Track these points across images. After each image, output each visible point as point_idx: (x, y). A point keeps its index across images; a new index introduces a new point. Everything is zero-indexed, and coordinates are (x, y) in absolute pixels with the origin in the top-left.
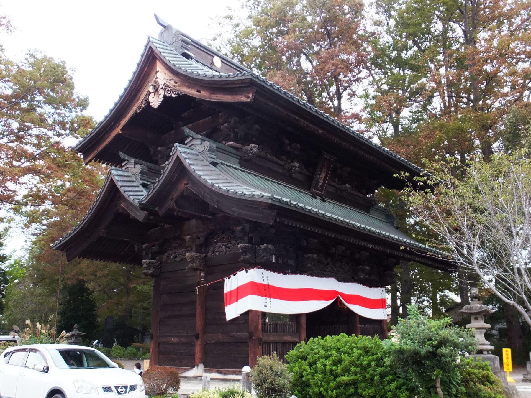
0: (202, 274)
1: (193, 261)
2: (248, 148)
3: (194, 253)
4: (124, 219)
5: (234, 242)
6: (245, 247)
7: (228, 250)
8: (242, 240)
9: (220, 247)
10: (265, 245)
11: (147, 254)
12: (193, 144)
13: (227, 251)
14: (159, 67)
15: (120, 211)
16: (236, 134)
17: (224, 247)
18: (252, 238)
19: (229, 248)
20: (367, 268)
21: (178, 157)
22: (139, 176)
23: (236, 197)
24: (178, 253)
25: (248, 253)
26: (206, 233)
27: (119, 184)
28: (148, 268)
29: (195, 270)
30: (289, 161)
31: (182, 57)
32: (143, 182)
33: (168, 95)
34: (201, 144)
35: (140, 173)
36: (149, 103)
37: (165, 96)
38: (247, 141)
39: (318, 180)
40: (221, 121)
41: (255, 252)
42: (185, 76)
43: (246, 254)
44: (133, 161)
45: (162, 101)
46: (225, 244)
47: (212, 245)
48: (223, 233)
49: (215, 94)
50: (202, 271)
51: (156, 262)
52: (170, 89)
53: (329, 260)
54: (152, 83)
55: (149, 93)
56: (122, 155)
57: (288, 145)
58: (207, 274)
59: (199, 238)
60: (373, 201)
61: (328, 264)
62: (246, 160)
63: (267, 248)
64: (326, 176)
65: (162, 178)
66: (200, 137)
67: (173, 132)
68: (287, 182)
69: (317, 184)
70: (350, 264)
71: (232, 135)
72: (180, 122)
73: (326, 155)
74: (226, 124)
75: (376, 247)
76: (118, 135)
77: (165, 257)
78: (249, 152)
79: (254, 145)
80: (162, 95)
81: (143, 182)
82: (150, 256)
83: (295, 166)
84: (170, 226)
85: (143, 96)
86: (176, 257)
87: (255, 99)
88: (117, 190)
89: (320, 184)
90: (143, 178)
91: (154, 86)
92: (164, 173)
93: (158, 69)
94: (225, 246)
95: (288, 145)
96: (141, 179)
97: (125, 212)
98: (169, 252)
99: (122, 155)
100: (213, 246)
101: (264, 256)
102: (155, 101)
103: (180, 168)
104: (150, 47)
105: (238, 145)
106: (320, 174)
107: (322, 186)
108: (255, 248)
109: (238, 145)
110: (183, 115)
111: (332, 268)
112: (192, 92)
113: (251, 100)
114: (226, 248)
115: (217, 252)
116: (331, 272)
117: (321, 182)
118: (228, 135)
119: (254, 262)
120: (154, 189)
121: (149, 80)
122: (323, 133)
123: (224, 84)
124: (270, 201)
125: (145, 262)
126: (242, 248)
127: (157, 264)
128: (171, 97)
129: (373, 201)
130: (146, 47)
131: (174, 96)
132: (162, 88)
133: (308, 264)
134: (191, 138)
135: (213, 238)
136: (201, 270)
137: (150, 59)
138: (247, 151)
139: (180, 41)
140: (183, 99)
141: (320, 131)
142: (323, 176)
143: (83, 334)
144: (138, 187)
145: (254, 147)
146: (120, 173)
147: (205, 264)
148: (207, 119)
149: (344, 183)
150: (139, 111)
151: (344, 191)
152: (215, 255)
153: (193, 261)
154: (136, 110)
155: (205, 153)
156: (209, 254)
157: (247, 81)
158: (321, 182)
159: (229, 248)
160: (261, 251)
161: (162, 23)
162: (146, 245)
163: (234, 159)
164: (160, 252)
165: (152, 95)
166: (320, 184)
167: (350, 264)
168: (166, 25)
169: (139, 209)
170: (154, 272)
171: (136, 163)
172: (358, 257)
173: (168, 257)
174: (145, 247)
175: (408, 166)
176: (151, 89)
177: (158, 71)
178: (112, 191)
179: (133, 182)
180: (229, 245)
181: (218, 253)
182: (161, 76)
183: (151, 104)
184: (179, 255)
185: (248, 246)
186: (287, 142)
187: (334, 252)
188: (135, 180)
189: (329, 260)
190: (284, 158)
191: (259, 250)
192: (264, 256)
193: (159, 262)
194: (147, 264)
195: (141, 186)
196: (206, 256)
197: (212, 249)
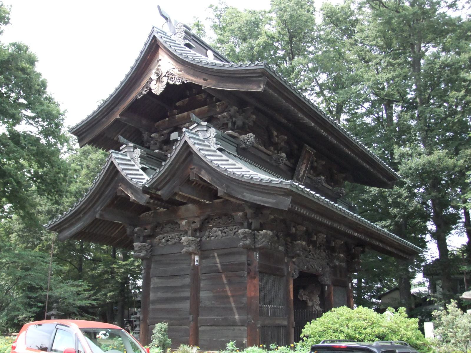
0: (197, 258)
1: (189, 245)
2: (245, 137)
3: (191, 238)
4: (121, 203)
5: (231, 227)
6: (246, 233)
7: (224, 234)
8: (241, 225)
9: (216, 232)
10: (264, 231)
11: (139, 237)
12: (198, 130)
13: (223, 236)
14: (163, 56)
15: (118, 194)
16: (234, 123)
17: (220, 232)
18: (251, 224)
19: (225, 233)
20: (342, 255)
21: (186, 142)
22: (138, 160)
23: (251, 182)
24: (171, 236)
25: (248, 238)
26: (202, 218)
27: (120, 168)
28: (140, 251)
29: (190, 254)
30: (276, 152)
31: (185, 47)
32: (143, 166)
33: (171, 83)
34: (207, 131)
35: (140, 157)
36: (150, 89)
37: (168, 84)
38: (243, 130)
39: (299, 171)
40: (218, 110)
41: (254, 238)
42: (192, 65)
43: (247, 240)
44: (132, 145)
45: (165, 89)
46: (221, 229)
47: (206, 230)
48: (220, 218)
49: (222, 83)
50: (197, 255)
51: (148, 246)
52: (173, 77)
53: (311, 247)
54: (154, 71)
55: (151, 80)
56: (122, 139)
57: (276, 136)
58: (201, 258)
59: (194, 222)
60: (341, 193)
61: (310, 251)
62: (244, 149)
63: (266, 234)
64: (306, 168)
65: (169, 162)
66: (206, 123)
67: (167, 119)
68: (275, 172)
69: (299, 175)
70: (327, 252)
71: (230, 125)
72: (174, 111)
73: (308, 148)
74: (225, 114)
75: (360, 236)
76: (117, 120)
77: (156, 240)
78: (246, 141)
79: (251, 134)
80: (165, 83)
81: (143, 166)
82: (141, 239)
83: (282, 157)
84: (165, 210)
85: (144, 83)
86: (168, 241)
87: (265, 90)
88: (117, 172)
89: (301, 175)
90: (142, 162)
91: (157, 74)
92: (171, 157)
93: (160, 57)
94: (222, 231)
95: (276, 136)
96: (141, 163)
97: (123, 194)
98: (161, 236)
99: (122, 139)
100: (208, 230)
101: (263, 242)
102: (157, 89)
103: (187, 152)
104: (154, 36)
105: (236, 134)
106: (302, 165)
107: (302, 177)
108: (254, 234)
109: (236, 134)
110: (177, 104)
111: (313, 255)
112: (198, 81)
113: (262, 90)
114: (222, 233)
115: (212, 236)
116: (313, 259)
117: (302, 173)
118: (227, 124)
119: (253, 247)
120: (159, 172)
121: (152, 67)
122: (314, 126)
123: (234, 74)
124: (288, 187)
125: (137, 245)
126: (243, 234)
127: (148, 248)
128: (174, 85)
129: (341, 193)
130: (150, 36)
131: (177, 83)
132: (165, 76)
133: (297, 250)
134: (196, 125)
135: (208, 222)
136: (195, 254)
137: (153, 48)
138: (244, 140)
139: (183, 32)
140: (187, 87)
141: (313, 124)
142: (303, 167)
143: (62, 314)
144: (138, 170)
145: (250, 137)
146: (120, 156)
147: (199, 249)
148: (203, 108)
149: (318, 175)
150: (139, 97)
151: (319, 182)
152: (211, 240)
153: (189, 245)
154: (137, 96)
155: (211, 140)
156: (204, 239)
157: (259, 71)
158: (302, 173)
159: (225, 233)
160: (260, 237)
161: (163, 14)
162: (139, 228)
163: (233, 147)
164: (151, 236)
165: (154, 82)
166: (301, 175)
167: (327, 252)
168: (167, 17)
169: (141, 192)
170: (146, 255)
171: (135, 148)
172: (333, 245)
173: (160, 240)
174: (138, 230)
175: (377, 161)
176: (154, 77)
177: (161, 60)
178: (113, 173)
179: (133, 165)
180: (226, 230)
181: (213, 238)
182: (165, 64)
183: (152, 91)
184: (171, 239)
185: (249, 231)
186: (275, 133)
187: (315, 239)
188: (134, 163)
189: (311, 247)
190: (272, 148)
191: (259, 236)
192: (263, 242)
193: (150, 245)
194: (139, 247)
195: (140, 170)
196: (200, 240)
197: (207, 233)
